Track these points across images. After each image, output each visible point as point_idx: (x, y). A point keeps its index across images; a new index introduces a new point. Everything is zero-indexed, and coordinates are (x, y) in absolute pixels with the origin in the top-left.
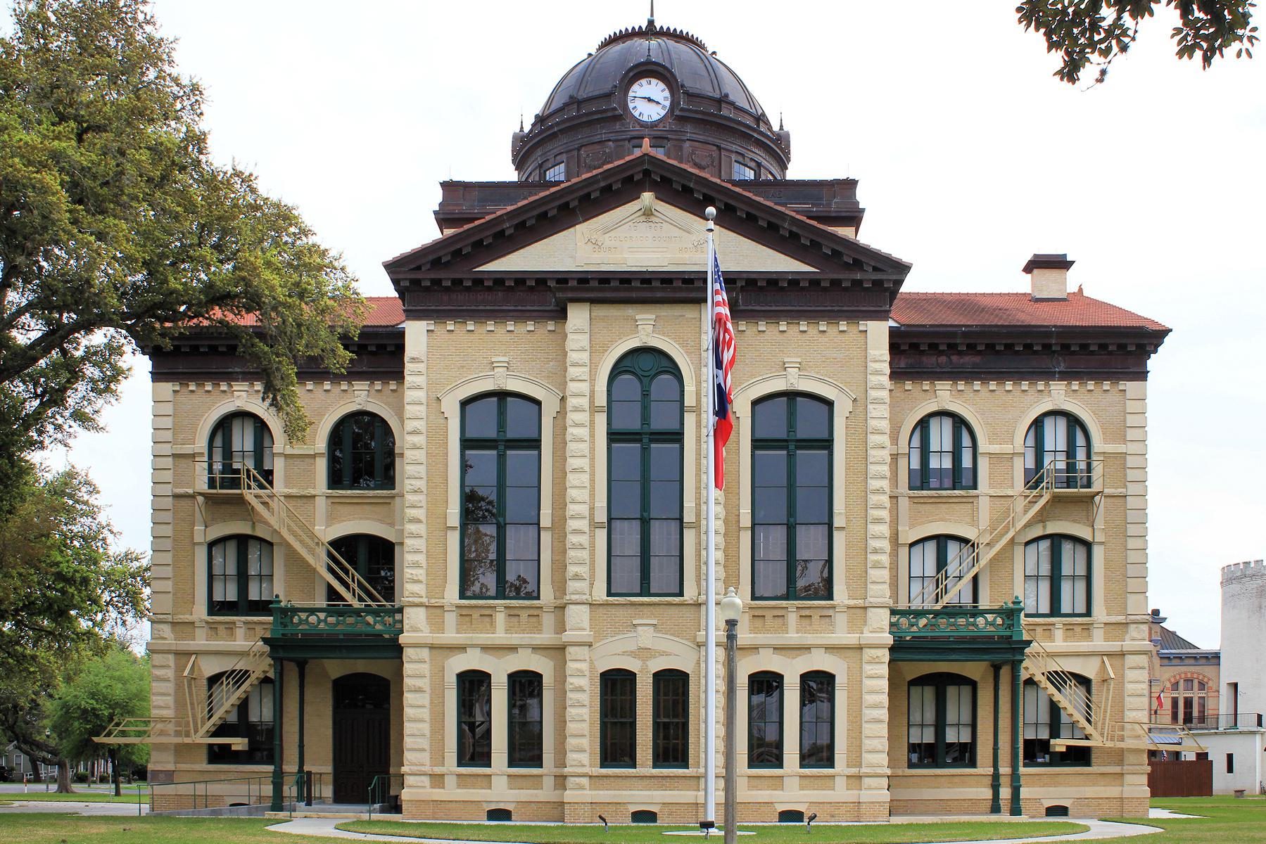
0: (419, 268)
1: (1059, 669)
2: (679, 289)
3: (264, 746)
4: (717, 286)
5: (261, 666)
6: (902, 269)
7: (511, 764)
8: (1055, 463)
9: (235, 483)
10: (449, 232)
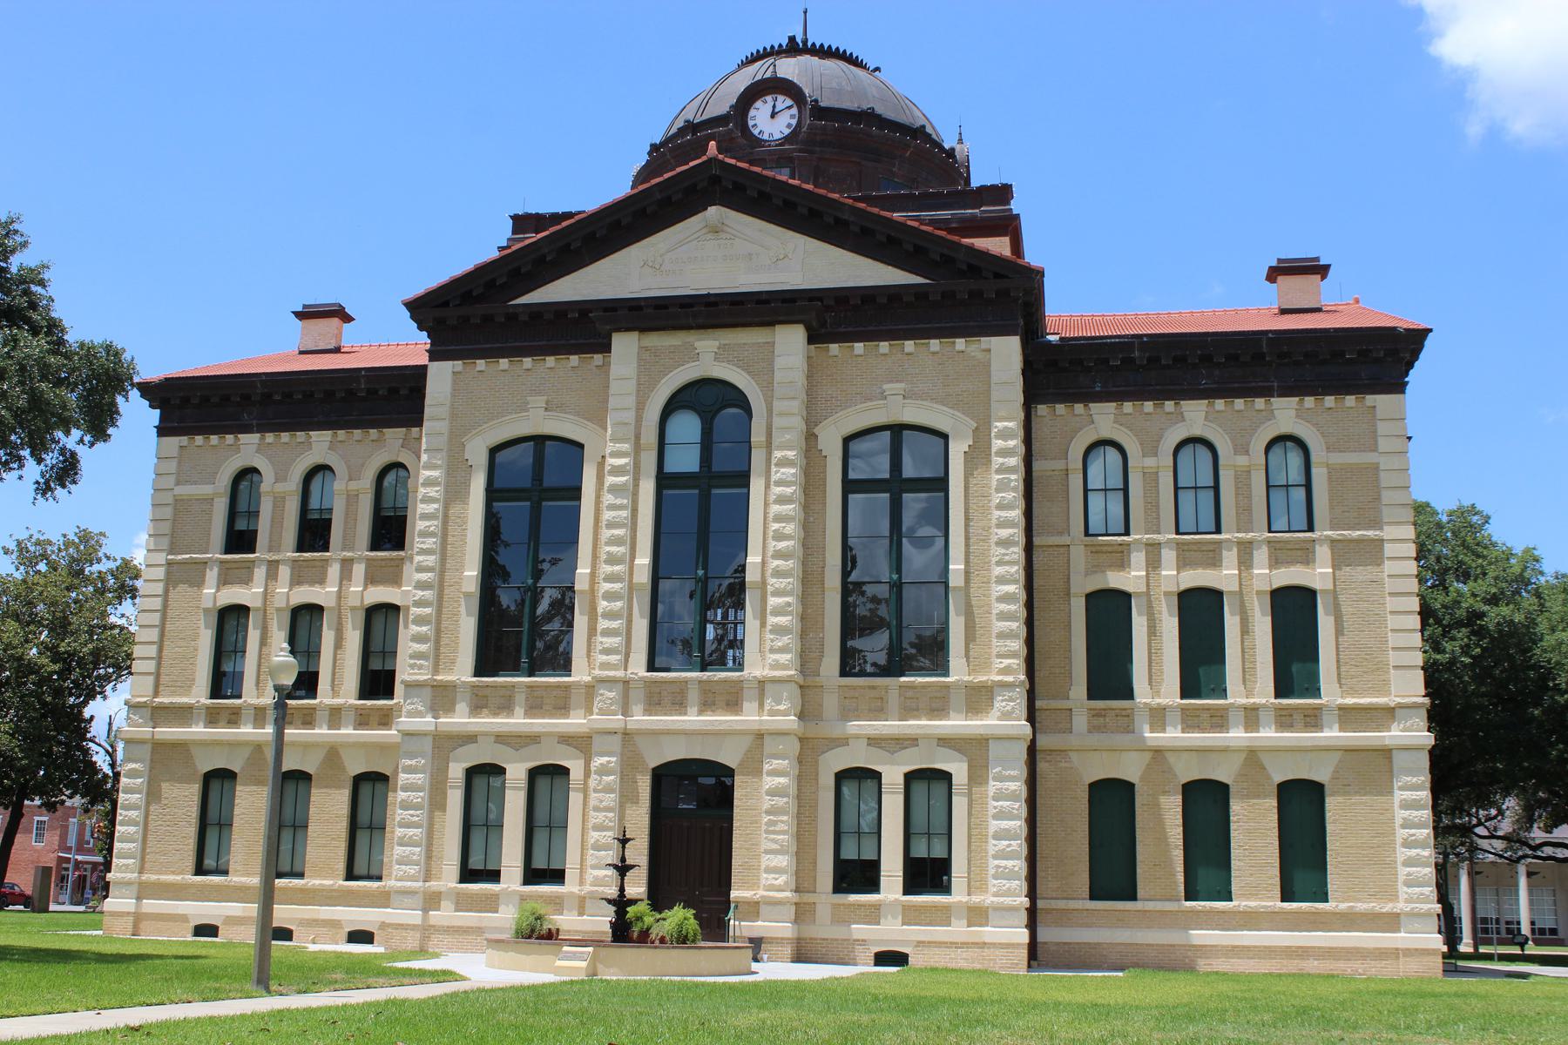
0: (446, 304)
7: (1091, 697)
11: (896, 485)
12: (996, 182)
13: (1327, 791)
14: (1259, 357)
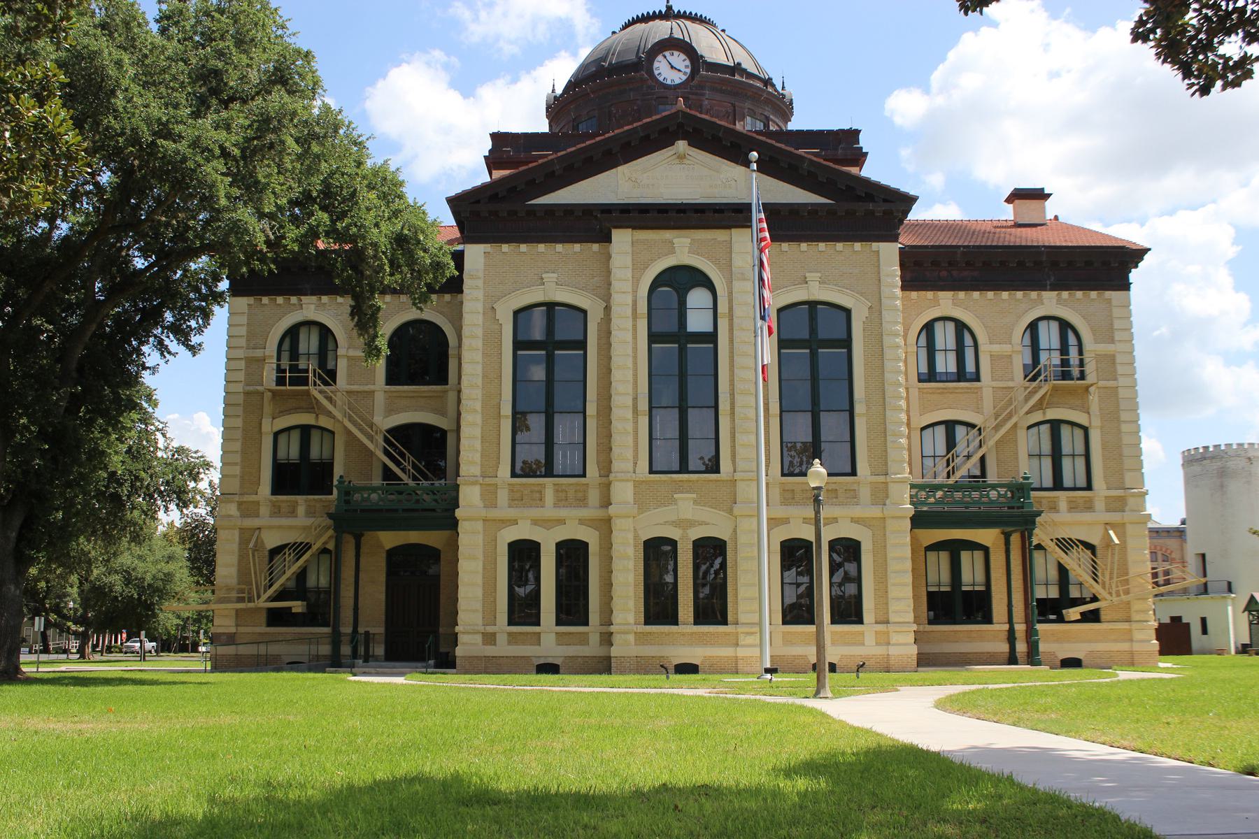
0: (478, 202)
1: (1066, 537)
2: (732, 215)
3: (320, 609)
4: (763, 216)
5: (325, 539)
6: (907, 201)
8: (1051, 359)
9: (305, 382)
10: (498, 174)
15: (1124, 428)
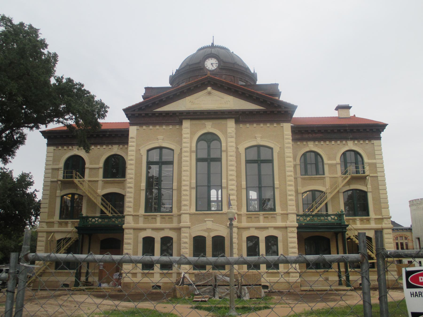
11: (259, 162)
12: (274, 83)
13: (331, 240)
14: (358, 131)
15: (381, 192)
